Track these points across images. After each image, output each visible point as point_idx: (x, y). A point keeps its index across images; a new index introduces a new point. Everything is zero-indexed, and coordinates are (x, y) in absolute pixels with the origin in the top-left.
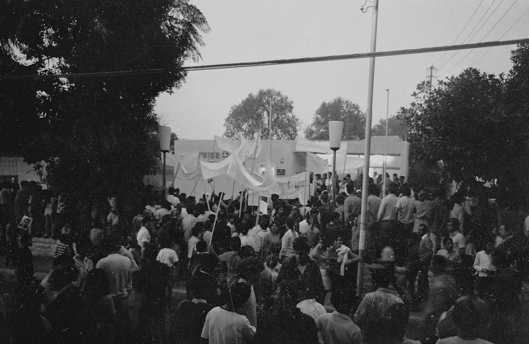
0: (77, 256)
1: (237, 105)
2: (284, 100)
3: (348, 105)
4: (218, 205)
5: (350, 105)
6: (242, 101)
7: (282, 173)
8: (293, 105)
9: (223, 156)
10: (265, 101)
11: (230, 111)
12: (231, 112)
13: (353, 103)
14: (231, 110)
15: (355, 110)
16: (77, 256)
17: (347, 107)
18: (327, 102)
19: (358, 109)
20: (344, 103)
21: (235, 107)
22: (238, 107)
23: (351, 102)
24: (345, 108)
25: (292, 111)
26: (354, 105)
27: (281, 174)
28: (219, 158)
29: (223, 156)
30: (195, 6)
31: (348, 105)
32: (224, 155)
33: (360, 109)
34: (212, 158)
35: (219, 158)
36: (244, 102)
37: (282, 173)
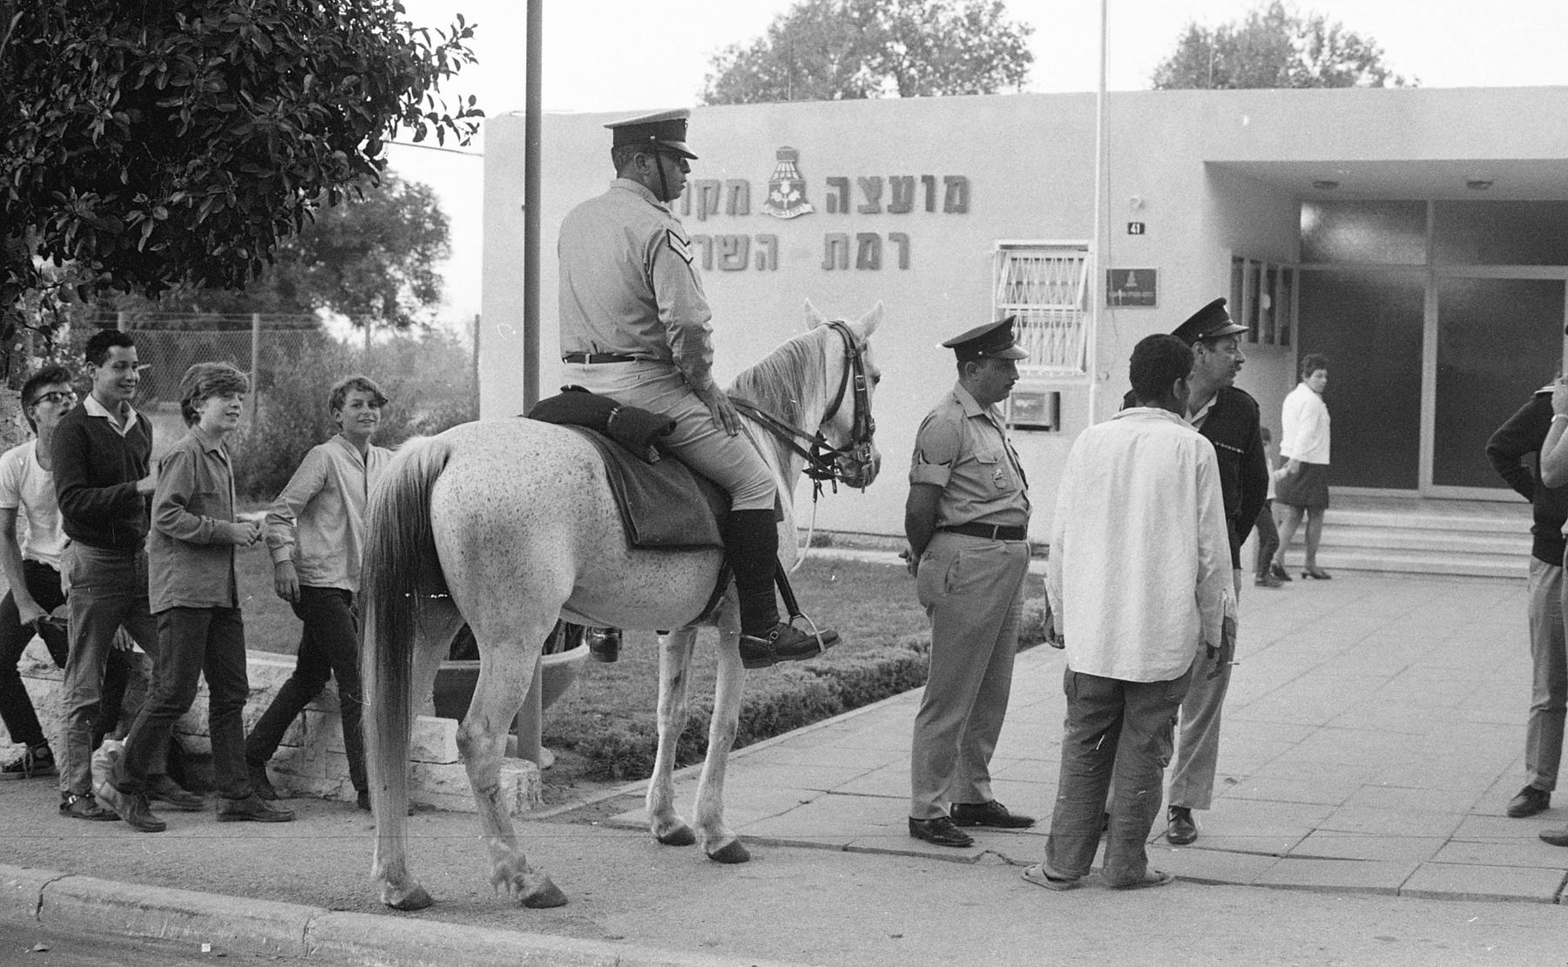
0: (1229, 324)
1: (746, 46)
2: (985, 20)
3: (1320, 39)
4: (1424, 220)
5: (1332, 39)
6: (770, 20)
7: (1137, 294)
8: (1030, 44)
9: (771, 202)
10: (886, 26)
11: (708, 77)
12: (714, 82)
13: (1347, 30)
14: (713, 70)
15: (1360, 69)
16: (1229, 324)
17: (1316, 53)
18: (1210, 24)
19: (1375, 59)
20: (1304, 28)
21: (733, 58)
22: (748, 58)
23: (1339, 26)
24: (1308, 61)
25: (1025, 77)
26: (1353, 41)
27: (1128, 302)
28: (747, 213)
29: (771, 202)
30: (448, 218)
31: (1320, 39)
32: (776, 196)
33: (1383, 63)
34: (703, 217)
35: (747, 213)
36: (781, 27)
37: (1137, 294)
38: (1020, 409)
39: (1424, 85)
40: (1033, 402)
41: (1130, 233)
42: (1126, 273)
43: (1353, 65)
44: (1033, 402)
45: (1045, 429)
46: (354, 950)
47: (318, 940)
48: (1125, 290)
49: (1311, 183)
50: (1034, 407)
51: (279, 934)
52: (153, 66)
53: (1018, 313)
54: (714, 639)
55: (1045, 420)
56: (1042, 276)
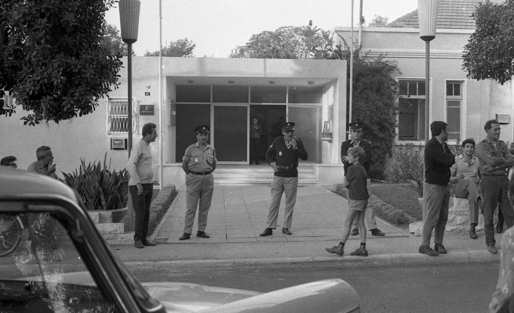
7: (148, 112)
27: (146, 114)
37: (148, 112)
38: (116, 144)
39: (216, 56)
40: (120, 142)
41: (146, 95)
42: (145, 106)
43: (110, 35)
44: (120, 142)
45: (123, 149)
46: (168, 269)
47: (157, 268)
48: (145, 111)
49: (186, 81)
50: (120, 143)
51: (147, 268)
52: (392, 108)
53: (115, 117)
54: (43, 216)
55: (124, 147)
56: (122, 106)
